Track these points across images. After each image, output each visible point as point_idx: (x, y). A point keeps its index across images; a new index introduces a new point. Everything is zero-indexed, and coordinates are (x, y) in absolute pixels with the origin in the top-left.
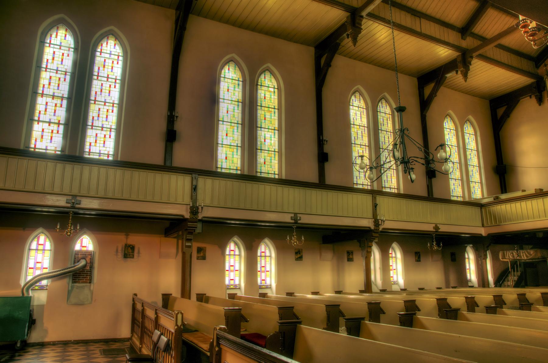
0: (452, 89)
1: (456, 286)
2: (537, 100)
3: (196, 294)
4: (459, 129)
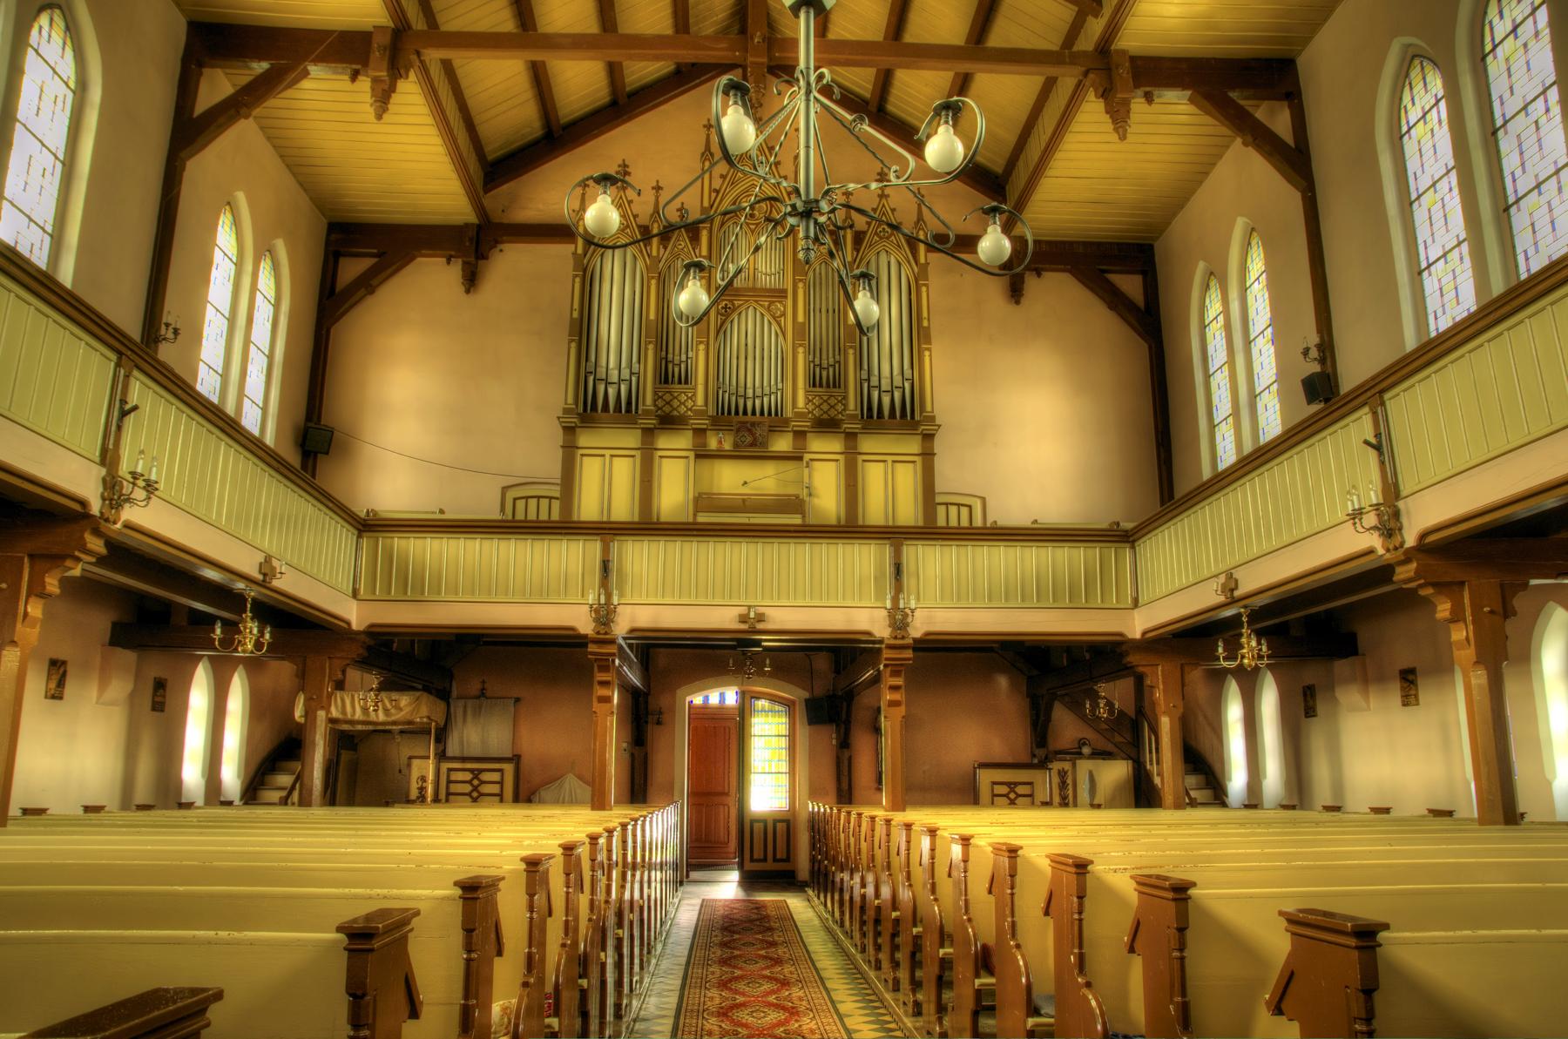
0: (262, 128)
1: (152, 804)
2: (464, 276)
3: (21, 808)
4: (249, 267)
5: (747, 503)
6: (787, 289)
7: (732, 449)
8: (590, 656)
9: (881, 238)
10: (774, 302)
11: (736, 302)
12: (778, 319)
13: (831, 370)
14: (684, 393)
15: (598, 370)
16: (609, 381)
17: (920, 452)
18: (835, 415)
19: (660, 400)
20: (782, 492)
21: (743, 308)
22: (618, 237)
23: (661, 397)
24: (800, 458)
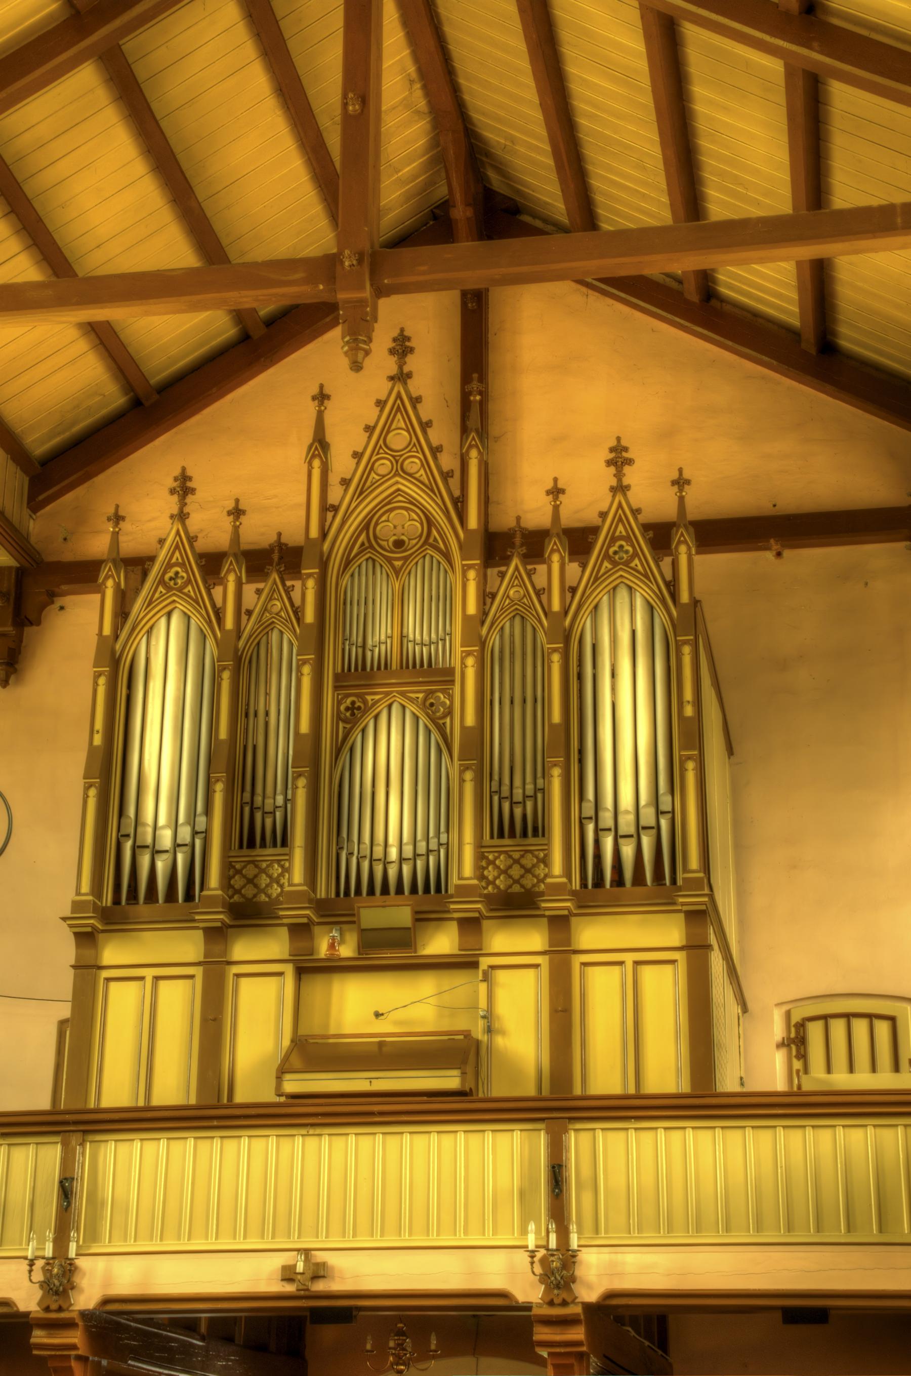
5: (385, 1049)
6: (454, 668)
7: (355, 955)
8: (35, 1352)
9: (615, 563)
10: (432, 692)
11: (369, 698)
12: (441, 722)
13: (529, 805)
14: (279, 861)
15: (139, 829)
16: (157, 848)
17: (684, 943)
18: (534, 886)
19: (237, 877)
20: (446, 1026)
21: (383, 706)
22: (174, 601)
23: (238, 872)
24: (474, 965)
